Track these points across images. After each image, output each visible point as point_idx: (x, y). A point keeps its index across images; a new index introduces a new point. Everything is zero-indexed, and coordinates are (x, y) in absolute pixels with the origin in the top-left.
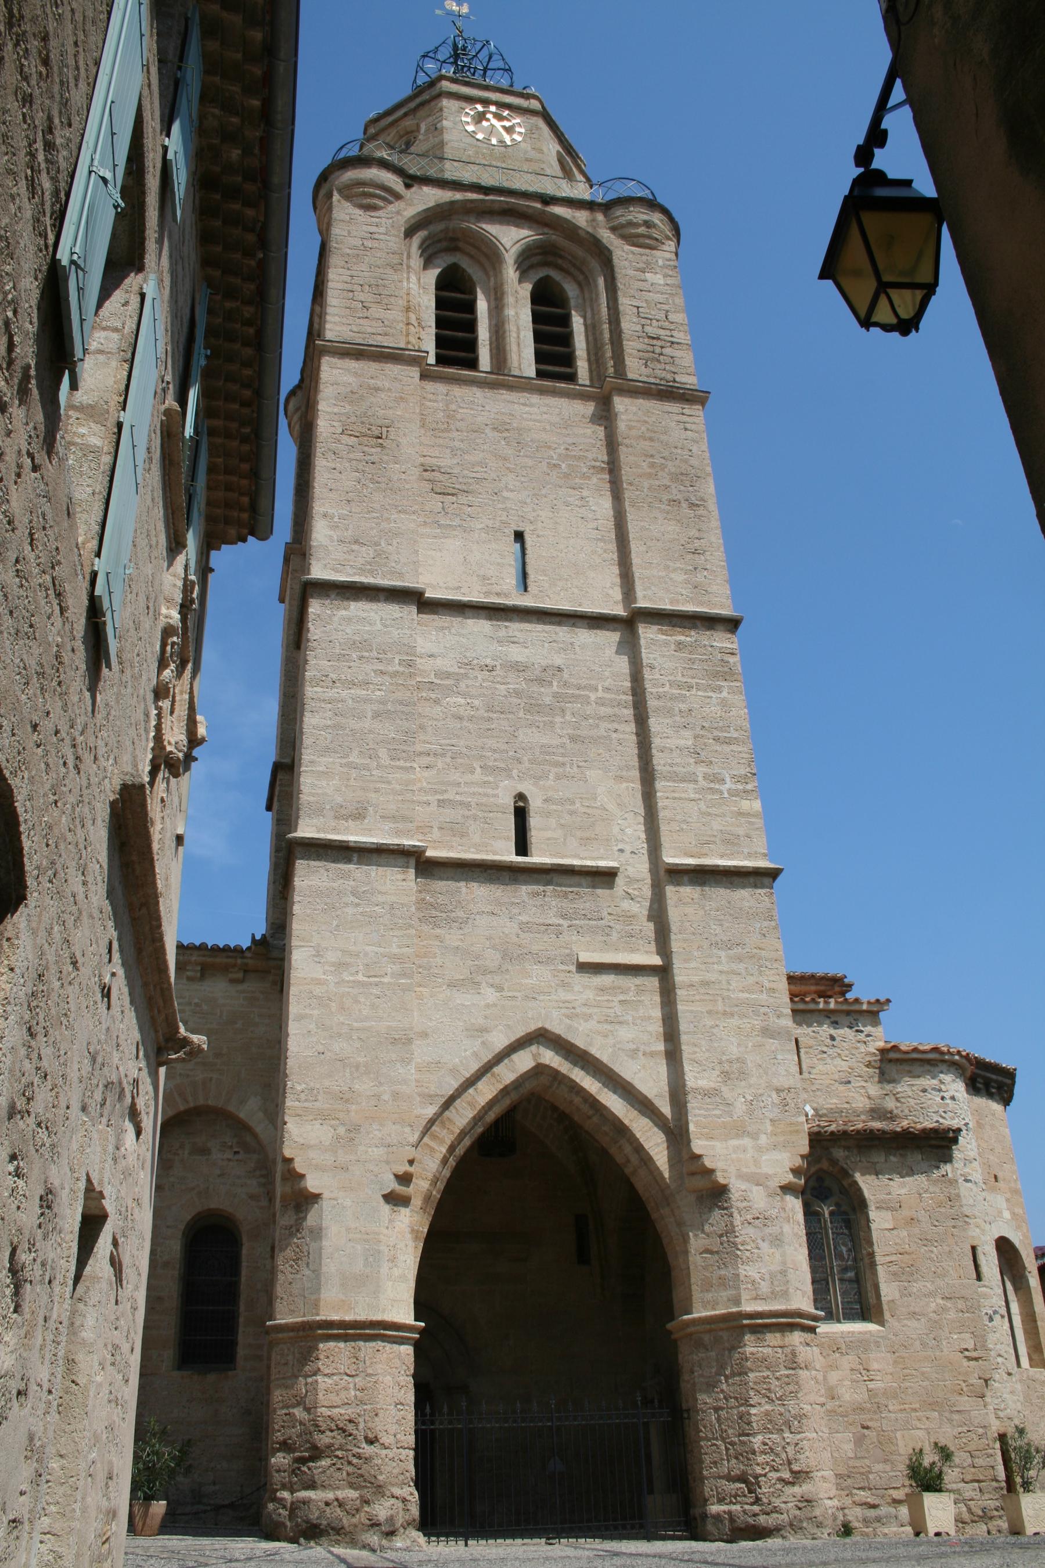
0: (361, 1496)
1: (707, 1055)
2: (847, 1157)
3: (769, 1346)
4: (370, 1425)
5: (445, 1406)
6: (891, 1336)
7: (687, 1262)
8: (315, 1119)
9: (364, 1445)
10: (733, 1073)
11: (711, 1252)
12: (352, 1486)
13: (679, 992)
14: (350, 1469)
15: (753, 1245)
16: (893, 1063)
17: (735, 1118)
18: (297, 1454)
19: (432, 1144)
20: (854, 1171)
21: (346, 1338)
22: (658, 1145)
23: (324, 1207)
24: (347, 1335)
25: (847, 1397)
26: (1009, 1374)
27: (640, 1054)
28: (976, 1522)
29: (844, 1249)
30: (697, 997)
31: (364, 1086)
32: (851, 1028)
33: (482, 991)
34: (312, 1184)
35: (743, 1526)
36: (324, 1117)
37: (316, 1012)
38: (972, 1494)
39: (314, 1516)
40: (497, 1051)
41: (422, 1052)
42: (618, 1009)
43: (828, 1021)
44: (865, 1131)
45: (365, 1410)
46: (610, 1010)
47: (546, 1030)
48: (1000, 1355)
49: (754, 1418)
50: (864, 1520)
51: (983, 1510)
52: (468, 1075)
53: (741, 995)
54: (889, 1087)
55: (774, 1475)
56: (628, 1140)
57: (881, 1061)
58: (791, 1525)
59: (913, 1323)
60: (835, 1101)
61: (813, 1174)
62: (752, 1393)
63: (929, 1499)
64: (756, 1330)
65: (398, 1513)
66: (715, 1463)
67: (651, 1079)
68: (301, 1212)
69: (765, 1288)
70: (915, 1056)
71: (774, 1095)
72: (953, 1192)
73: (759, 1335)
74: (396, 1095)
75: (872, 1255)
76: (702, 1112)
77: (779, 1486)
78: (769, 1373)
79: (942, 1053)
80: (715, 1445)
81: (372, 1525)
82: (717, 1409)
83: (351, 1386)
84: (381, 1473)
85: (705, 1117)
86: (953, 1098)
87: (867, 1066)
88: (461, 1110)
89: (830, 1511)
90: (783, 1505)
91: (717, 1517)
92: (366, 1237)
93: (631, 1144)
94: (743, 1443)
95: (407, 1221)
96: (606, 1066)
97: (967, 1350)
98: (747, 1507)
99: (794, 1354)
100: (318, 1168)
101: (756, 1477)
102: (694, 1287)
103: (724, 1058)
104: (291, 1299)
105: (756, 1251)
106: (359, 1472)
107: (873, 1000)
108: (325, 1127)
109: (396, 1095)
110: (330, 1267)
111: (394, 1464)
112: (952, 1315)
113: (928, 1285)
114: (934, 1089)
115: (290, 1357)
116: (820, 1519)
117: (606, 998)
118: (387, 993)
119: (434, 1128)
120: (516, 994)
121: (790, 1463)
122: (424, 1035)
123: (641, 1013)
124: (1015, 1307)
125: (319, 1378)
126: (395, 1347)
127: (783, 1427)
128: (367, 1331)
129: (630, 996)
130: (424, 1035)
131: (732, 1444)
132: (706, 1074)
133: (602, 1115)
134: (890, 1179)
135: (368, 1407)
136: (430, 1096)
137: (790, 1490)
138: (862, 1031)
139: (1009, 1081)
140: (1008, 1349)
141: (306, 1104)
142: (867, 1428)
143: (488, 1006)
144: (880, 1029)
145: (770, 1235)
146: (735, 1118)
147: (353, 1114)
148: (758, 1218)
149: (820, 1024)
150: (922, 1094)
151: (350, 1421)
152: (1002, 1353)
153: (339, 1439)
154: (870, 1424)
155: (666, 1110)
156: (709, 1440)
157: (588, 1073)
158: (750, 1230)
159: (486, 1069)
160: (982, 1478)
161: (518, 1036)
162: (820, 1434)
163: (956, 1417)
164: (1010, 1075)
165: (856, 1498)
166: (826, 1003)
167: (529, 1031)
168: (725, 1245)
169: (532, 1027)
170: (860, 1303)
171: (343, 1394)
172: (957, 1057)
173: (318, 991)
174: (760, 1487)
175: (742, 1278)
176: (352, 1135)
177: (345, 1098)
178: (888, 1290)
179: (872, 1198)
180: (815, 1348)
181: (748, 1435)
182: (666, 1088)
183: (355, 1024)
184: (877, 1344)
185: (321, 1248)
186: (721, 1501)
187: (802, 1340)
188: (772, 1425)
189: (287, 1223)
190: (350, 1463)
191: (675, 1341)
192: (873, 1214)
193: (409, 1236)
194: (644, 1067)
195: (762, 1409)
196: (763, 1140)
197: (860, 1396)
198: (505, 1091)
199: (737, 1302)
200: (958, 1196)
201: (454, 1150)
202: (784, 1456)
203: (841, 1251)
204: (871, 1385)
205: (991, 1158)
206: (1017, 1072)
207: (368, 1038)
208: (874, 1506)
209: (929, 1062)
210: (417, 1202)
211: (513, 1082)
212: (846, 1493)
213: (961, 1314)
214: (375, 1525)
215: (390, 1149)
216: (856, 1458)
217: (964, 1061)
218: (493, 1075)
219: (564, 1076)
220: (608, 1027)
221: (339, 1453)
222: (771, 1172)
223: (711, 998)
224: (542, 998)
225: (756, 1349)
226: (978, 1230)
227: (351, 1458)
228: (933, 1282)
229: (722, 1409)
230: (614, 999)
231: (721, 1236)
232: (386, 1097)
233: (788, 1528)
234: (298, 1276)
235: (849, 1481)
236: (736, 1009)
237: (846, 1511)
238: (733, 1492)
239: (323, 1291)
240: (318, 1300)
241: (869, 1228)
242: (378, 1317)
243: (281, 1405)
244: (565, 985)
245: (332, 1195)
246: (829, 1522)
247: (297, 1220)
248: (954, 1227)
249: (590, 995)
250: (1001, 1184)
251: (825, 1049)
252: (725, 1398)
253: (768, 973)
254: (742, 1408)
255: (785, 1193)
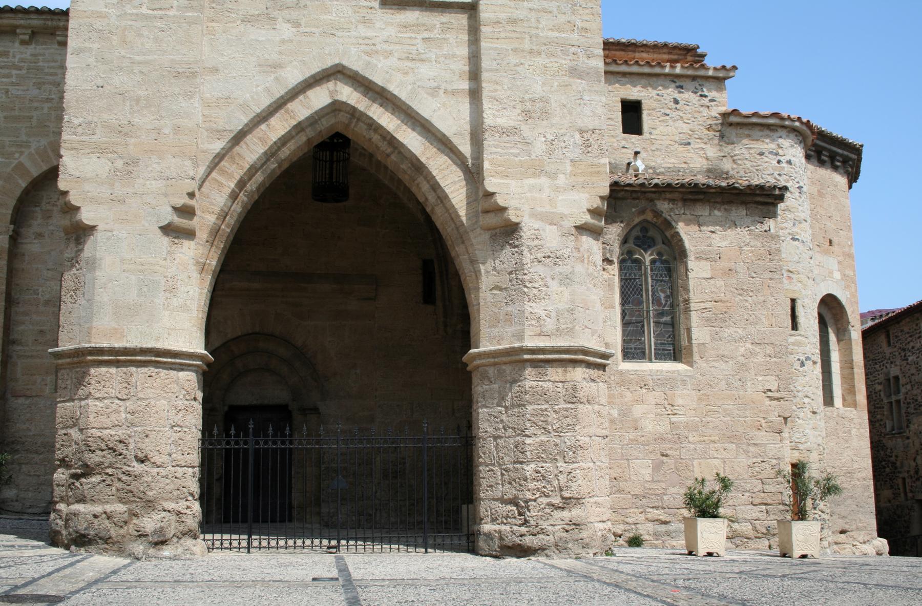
0: (129, 510)
1: (509, 93)
2: (671, 209)
3: (549, 380)
4: (139, 445)
5: (233, 429)
6: (698, 376)
7: (477, 298)
8: (92, 153)
9: (135, 464)
10: (535, 112)
11: (501, 289)
12: (121, 500)
13: (483, 29)
14: (119, 485)
15: (542, 283)
16: (734, 125)
17: (533, 157)
18: (73, 471)
19: (220, 179)
20: (677, 222)
21: (118, 364)
22: (454, 183)
23: (99, 237)
24: (118, 361)
25: (650, 428)
26: (814, 413)
27: (441, 92)
28: (759, 538)
29: (662, 295)
30: (503, 35)
31: (144, 120)
32: (696, 93)
33: (278, 27)
34: (87, 216)
35: (510, 544)
36: (101, 150)
37: (96, 46)
38: (759, 515)
39: (82, 527)
40: (291, 86)
41: (210, 87)
42: (421, 47)
43: (673, 85)
44: (690, 184)
45: (135, 432)
46: (412, 48)
47: (344, 67)
48: (807, 396)
49: (528, 448)
50: (655, 534)
51: (768, 528)
52: (258, 111)
53: (550, 33)
54: (728, 149)
55: (544, 500)
56: (426, 178)
57: (722, 124)
58: (556, 545)
59: (721, 365)
60: (673, 160)
61: (637, 225)
62: (528, 424)
63: (703, 524)
64: (535, 364)
65: (169, 525)
66: (491, 486)
67: (452, 119)
68: (80, 244)
69: (550, 325)
70: (754, 120)
71: (577, 136)
72: (774, 246)
73: (540, 370)
74: (177, 129)
75: (687, 301)
76: (499, 150)
77: (548, 510)
78: (547, 406)
79: (782, 119)
80: (492, 470)
81: (140, 536)
82: (496, 438)
83: (122, 409)
84: (151, 489)
85: (501, 155)
86: (789, 162)
87: (708, 129)
88: (252, 146)
89: (599, 534)
90: (550, 528)
91: (489, 536)
92: (140, 267)
93: (428, 182)
94: (517, 470)
95: (191, 253)
96: (404, 103)
97: (770, 390)
98: (515, 528)
99: (574, 388)
100: (93, 200)
101: (526, 502)
102: (482, 322)
103: (527, 97)
104: (70, 327)
105: (544, 289)
106: (128, 488)
107: (719, 66)
108: (103, 160)
109: (177, 129)
110: (103, 297)
111: (168, 481)
112: (760, 359)
113: (740, 331)
114: (770, 153)
115: (69, 382)
116: (587, 540)
117: (408, 35)
118: (172, 26)
119: (223, 163)
120: (313, 30)
121: (561, 490)
122: (215, 70)
123: (445, 50)
124: (835, 356)
125: (90, 402)
126: (173, 373)
127: (558, 457)
128: (138, 358)
129: (435, 34)
130: (215, 70)
131: (507, 470)
132: (506, 112)
133: (400, 152)
134: (713, 232)
135: (139, 429)
136: (218, 131)
137: (558, 514)
138: (706, 96)
139: (854, 157)
140: (815, 391)
141: (83, 138)
142: (667, 456)
143: (283, 42)
144: (725, 94)
145: (561, 273)
146: (533, 157)
147: (131, 147)
148: (549, 257)
149: (666, 88)
150: (758, 157)
151: (121, 442)
152: (809, 394)
153: (110, 458)
154: (669, 452)
155: (465, 148)
156: (487, 466)
157: (386, 110)
158: (540, 269)
159: (279, 105)
160: (769, 501)
161: (313, 72)
162: (598, 463)
163: (752, 449)
164: (857, 150)
165: (649, 516)
166: (672, 67)
167: (325, 67)
168: (514, 282)
169: (329, 63)
170: (673, 344)
171: (113, 417)
172: (797, 124)
173: (98, 24)
174: (529, 511)
175: (527, 315)
176: (130, 168)
177: (124, 131)
178: (699, 333)
179: (693, 249)
180: (601, 384)
181: (521, 463)
182: (468, 127)
183: (137, 58)
184: (684, 382)
185: (94, 279)
186: (494, 520)
187: (586, 376)
188: (545, 453)
189: (69, 256)
190: (119, 480)
191: (470, 373)
192: (691, 264)
193: (194, 268)
194: (444, 105)
195: (537, 440)
196: (562, 180)
197: (663, 428)
198: (299, 128)
199: (521, 337)
200: (779, 250)
201: (245, 186)
202: (556, 483)
203: (659, 297)
204: (674, 419)
205: (829, 224)
206: (864, 150)
207: (150, 71)
208: (665, 523)
209: (769, 127)
210: (202, 235)
211: (307, 119)
212: (640, 510)
213: (768, 359)
214: (142, 536)
215: (169, 182)
216: (653, 481)
217: (804, 128)
218: (287, 111)
219: (362, 114)
220: (409, 64)
221: (109, 471)
222: (566, 211)
223: (518, 35)
224: (340, 34)
225: (536, 383)
226: (799, 285)
227: (120, 476)
228: (744, 328)
229: (501, 437)
230: (417, 36)
231: (511, 273)
232: (166, 131)
233: (553, 548)
234: (76, 306)
235: (644, 500)
236: (544, 48)
237: (639, 526)
238: (505, 514)
239: (95, 319)
240: (90, 328)
241: (687, 276)
242: (160, 345)
243: (61, 425)
244: (365, 21)
245: (107, 227)
246: (598, 543)
247: (77, 252)
248: (771, 279)
249: (392, 31)
250: (835, 248)
251: (668, 112)
252: (504, 428)
253: (581, 12)
254: (518, 438)
255: (581, 234)
